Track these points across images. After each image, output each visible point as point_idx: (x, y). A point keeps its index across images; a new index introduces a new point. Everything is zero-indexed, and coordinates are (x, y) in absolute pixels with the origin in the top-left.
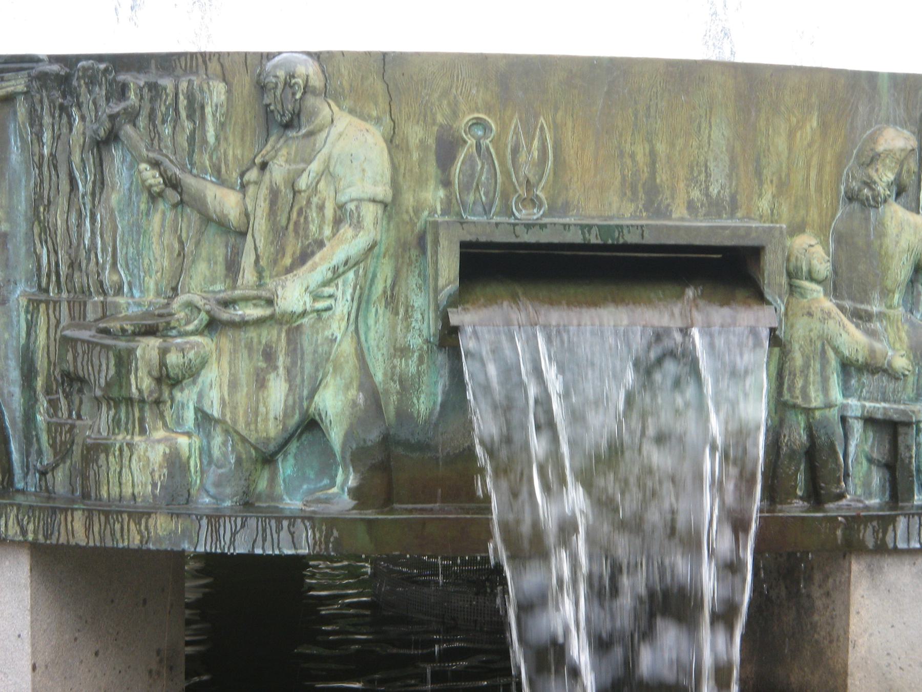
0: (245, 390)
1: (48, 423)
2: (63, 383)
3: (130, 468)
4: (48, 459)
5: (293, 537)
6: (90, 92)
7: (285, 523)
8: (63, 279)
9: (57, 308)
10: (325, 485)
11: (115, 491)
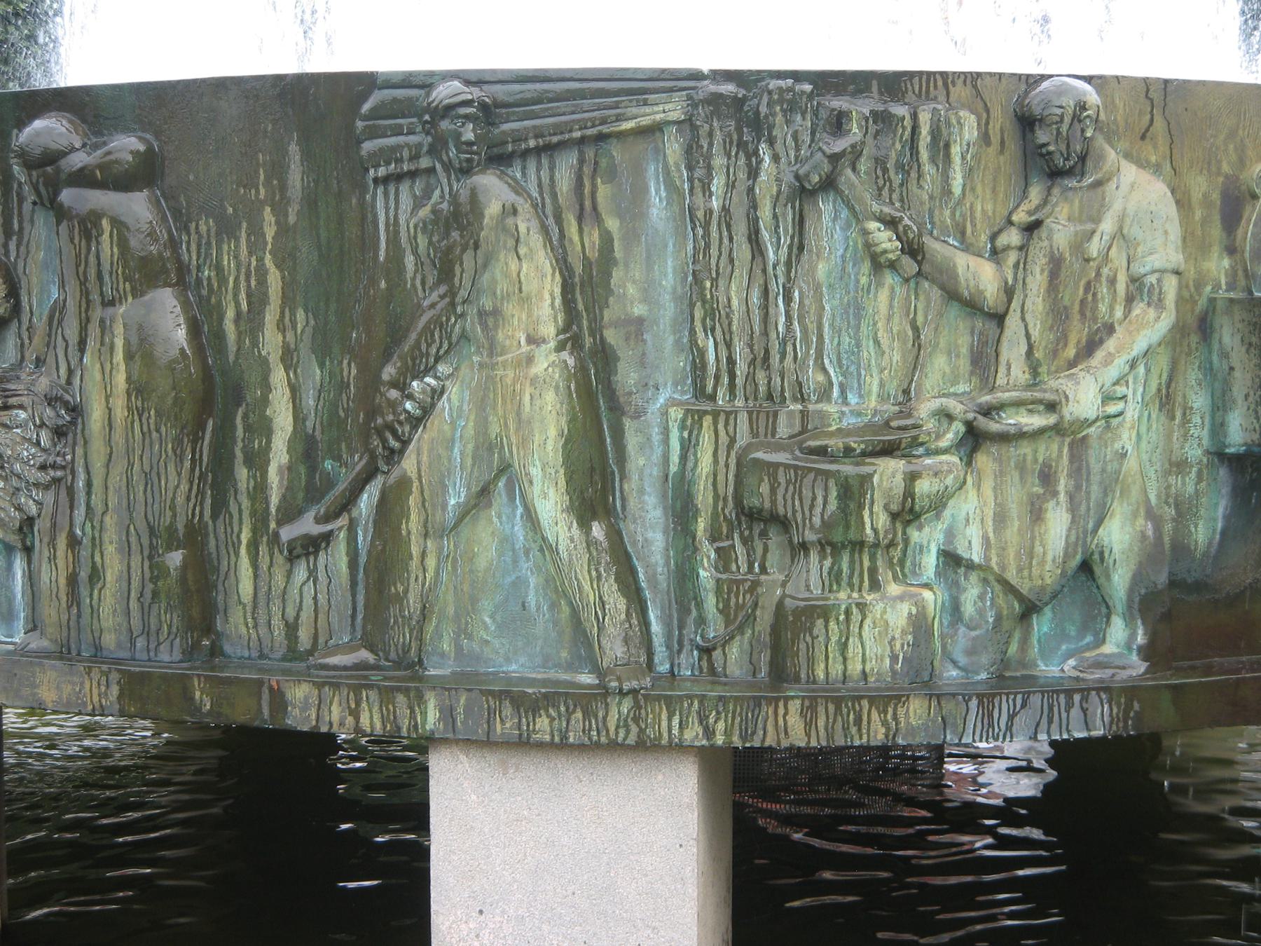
0: (1016, 523)
1: (718, 581)
2: (740, 524)
3: (861, 636)
4: (715, 630)
5: (1085, 715)
6: (788, 122)
7: (1077, 697)
8: (739, 381)
9: (732, 422)
10: (1088, 644)
11: (836, 669)
